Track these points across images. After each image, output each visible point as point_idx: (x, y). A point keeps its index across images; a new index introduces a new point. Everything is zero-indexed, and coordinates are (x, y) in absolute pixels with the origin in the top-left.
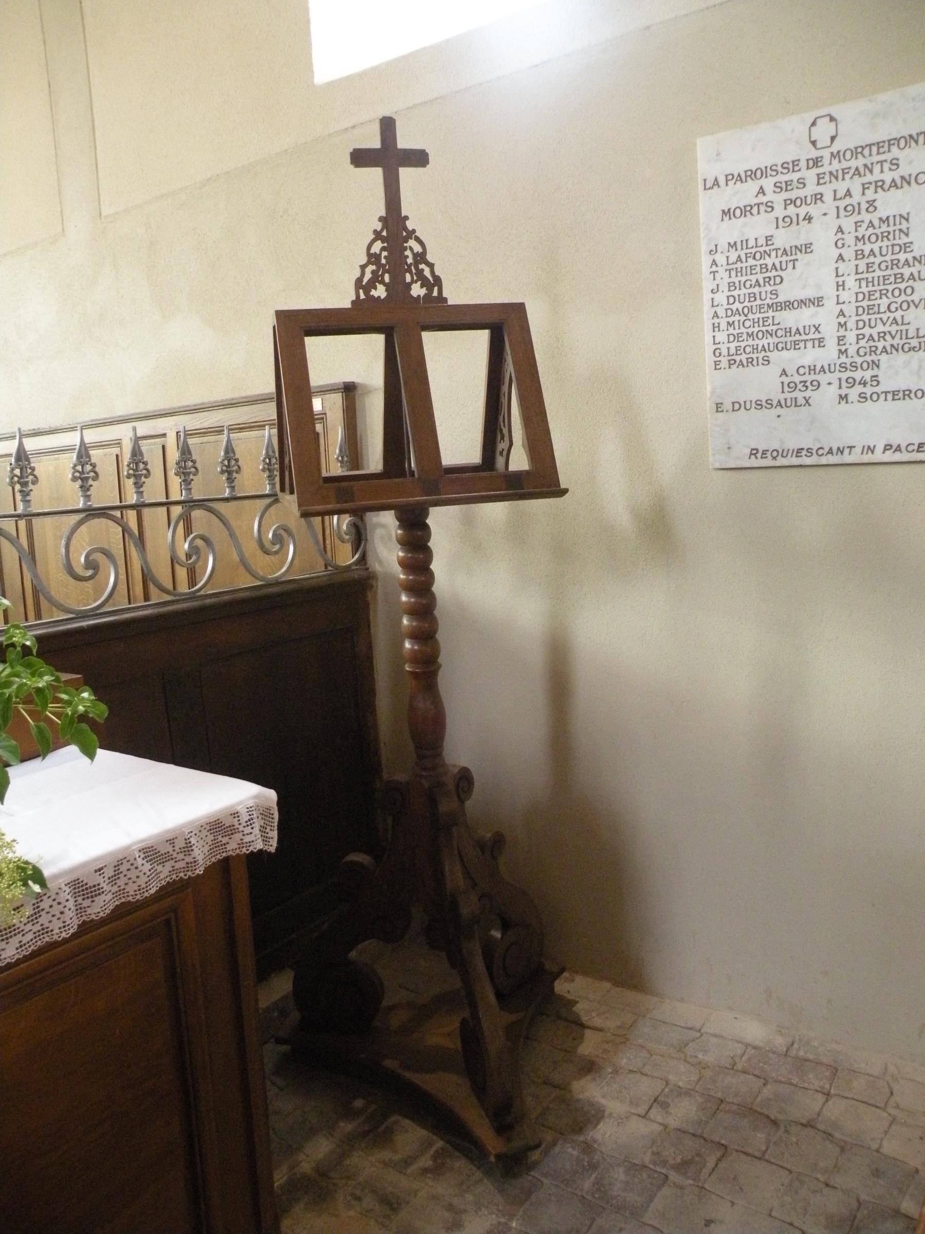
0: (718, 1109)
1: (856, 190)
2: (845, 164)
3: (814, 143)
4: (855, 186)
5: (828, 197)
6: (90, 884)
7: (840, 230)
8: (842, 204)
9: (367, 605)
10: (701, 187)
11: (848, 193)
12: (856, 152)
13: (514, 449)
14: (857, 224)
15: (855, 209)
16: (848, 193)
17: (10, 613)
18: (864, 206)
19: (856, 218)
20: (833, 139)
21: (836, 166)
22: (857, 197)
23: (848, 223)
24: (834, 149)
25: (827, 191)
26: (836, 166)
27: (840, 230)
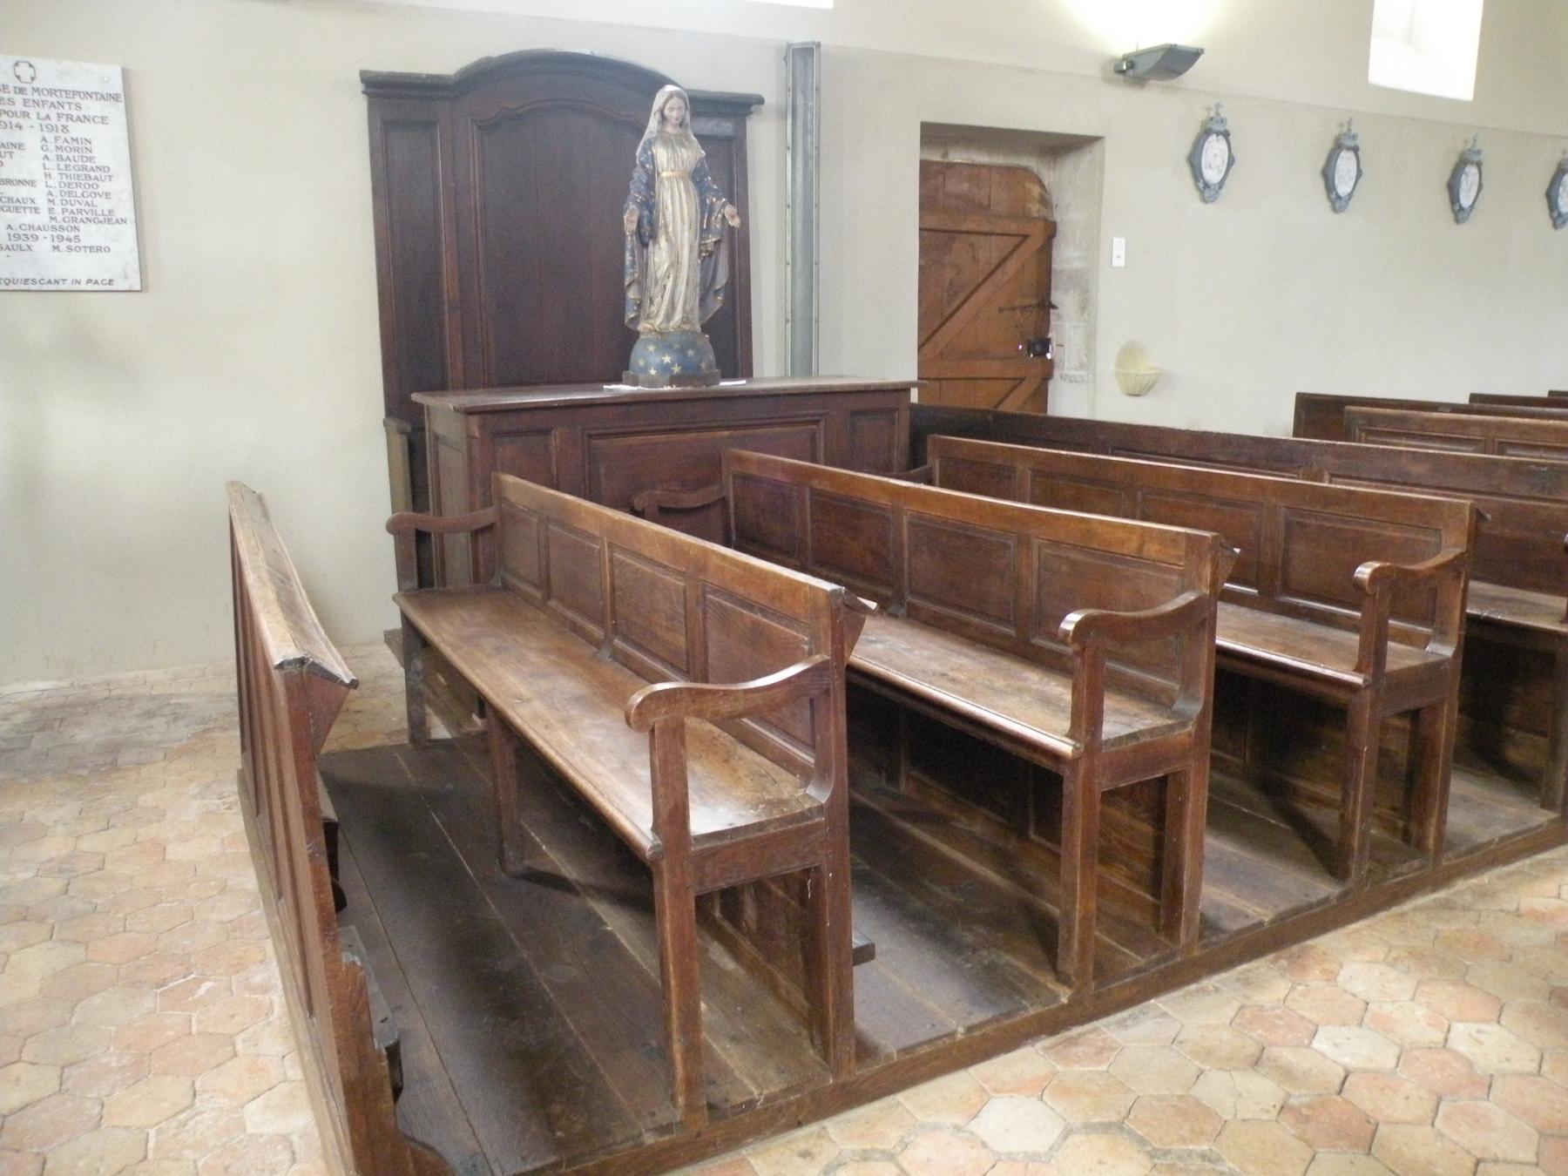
4: (53, 113)
5: (33, 116)
12: (51, 92)
14: (56, 139)
15: (53, 128)
18: (60, 128)
20: (33, 79)
21: (36, 97)
22: (54, 121)
23: (50, 136)
25: (32, 111)
26: (36, 97)
27: (44, 139)
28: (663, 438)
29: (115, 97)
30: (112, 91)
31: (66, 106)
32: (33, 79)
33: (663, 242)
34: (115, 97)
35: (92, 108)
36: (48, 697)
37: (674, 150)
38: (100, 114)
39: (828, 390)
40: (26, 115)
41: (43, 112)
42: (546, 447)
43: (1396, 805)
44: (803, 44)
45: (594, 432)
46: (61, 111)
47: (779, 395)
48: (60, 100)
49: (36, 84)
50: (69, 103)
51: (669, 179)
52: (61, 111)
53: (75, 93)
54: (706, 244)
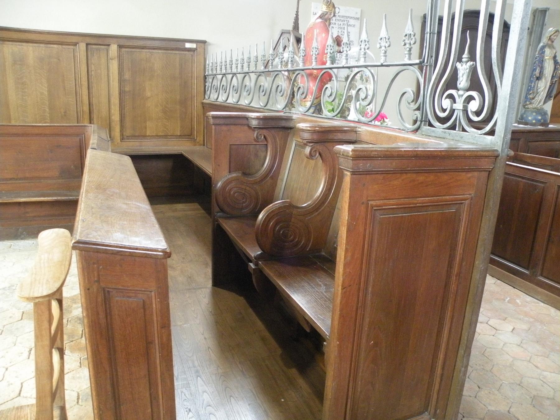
0: (522, 342)
1: (342, 25)
2: (340, 19)
3: (339, 8)
4: (342, 23)
5: (337, 24)
6: (193, 141)
7: (338, 32)
8: (339, 26)
9: (87, 310)
10: (312, 13)
11: (340, 25)
12: (343, 17)
13: (145, 198)
14: (341, 31)
15: (341, 28)
16: (340, 25)
17: (515, 329)
18: (343, 28)
19: (341, 30)
20: (339, 12)
21: (339, 18)
22: (342, 26)
23: (340, 31)
24: (339, 14)
25: (337, 22)
26: (339, 18)
27: (338, 32)
28: (544, 143)
29: (358, 19)
30: (357, 17)
31: (346, 21)
32: (339, 12)
33: (543, 80)
34: (358, 19)
35: (352, 22)
36: (276, 224)
37: (552, 50)
38: (353, 24)
39: (529, 131)
40: (335, 24)
41: (340, 23)
42: (518, 144)
43: (249, 403)
44: (542, 8)
45: (530, 140)
46: (344, 23)
47: (524, 132)
48: (344, 19)
49: (339, 14)
50: (346, 20)
51: (548, 59)
52: (344, 23)
53: (348, 17)
54: (553, 81)
